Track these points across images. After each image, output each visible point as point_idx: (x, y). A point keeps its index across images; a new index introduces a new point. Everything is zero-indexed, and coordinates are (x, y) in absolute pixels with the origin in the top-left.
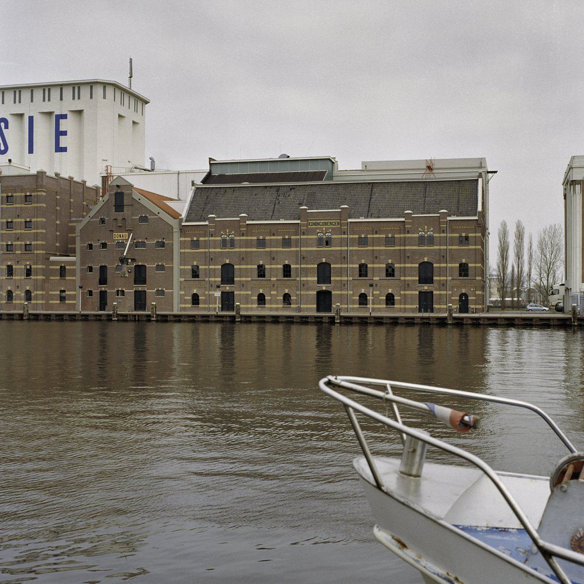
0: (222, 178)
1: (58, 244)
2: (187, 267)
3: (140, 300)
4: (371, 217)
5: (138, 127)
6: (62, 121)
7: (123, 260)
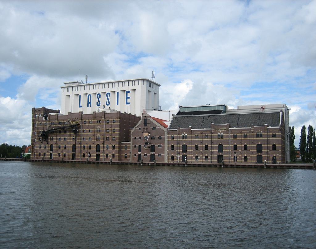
0: (184, 113)
1: (124, 137)
2: (255, 145)
3: (152, 157)
4: (238, 127)
5: (156, 95)
6: (129, 94)
7: (147, 143)
